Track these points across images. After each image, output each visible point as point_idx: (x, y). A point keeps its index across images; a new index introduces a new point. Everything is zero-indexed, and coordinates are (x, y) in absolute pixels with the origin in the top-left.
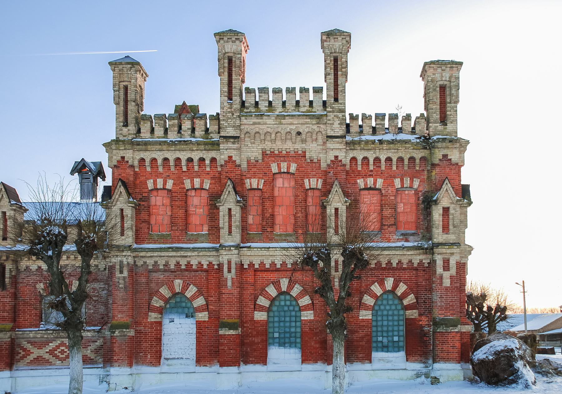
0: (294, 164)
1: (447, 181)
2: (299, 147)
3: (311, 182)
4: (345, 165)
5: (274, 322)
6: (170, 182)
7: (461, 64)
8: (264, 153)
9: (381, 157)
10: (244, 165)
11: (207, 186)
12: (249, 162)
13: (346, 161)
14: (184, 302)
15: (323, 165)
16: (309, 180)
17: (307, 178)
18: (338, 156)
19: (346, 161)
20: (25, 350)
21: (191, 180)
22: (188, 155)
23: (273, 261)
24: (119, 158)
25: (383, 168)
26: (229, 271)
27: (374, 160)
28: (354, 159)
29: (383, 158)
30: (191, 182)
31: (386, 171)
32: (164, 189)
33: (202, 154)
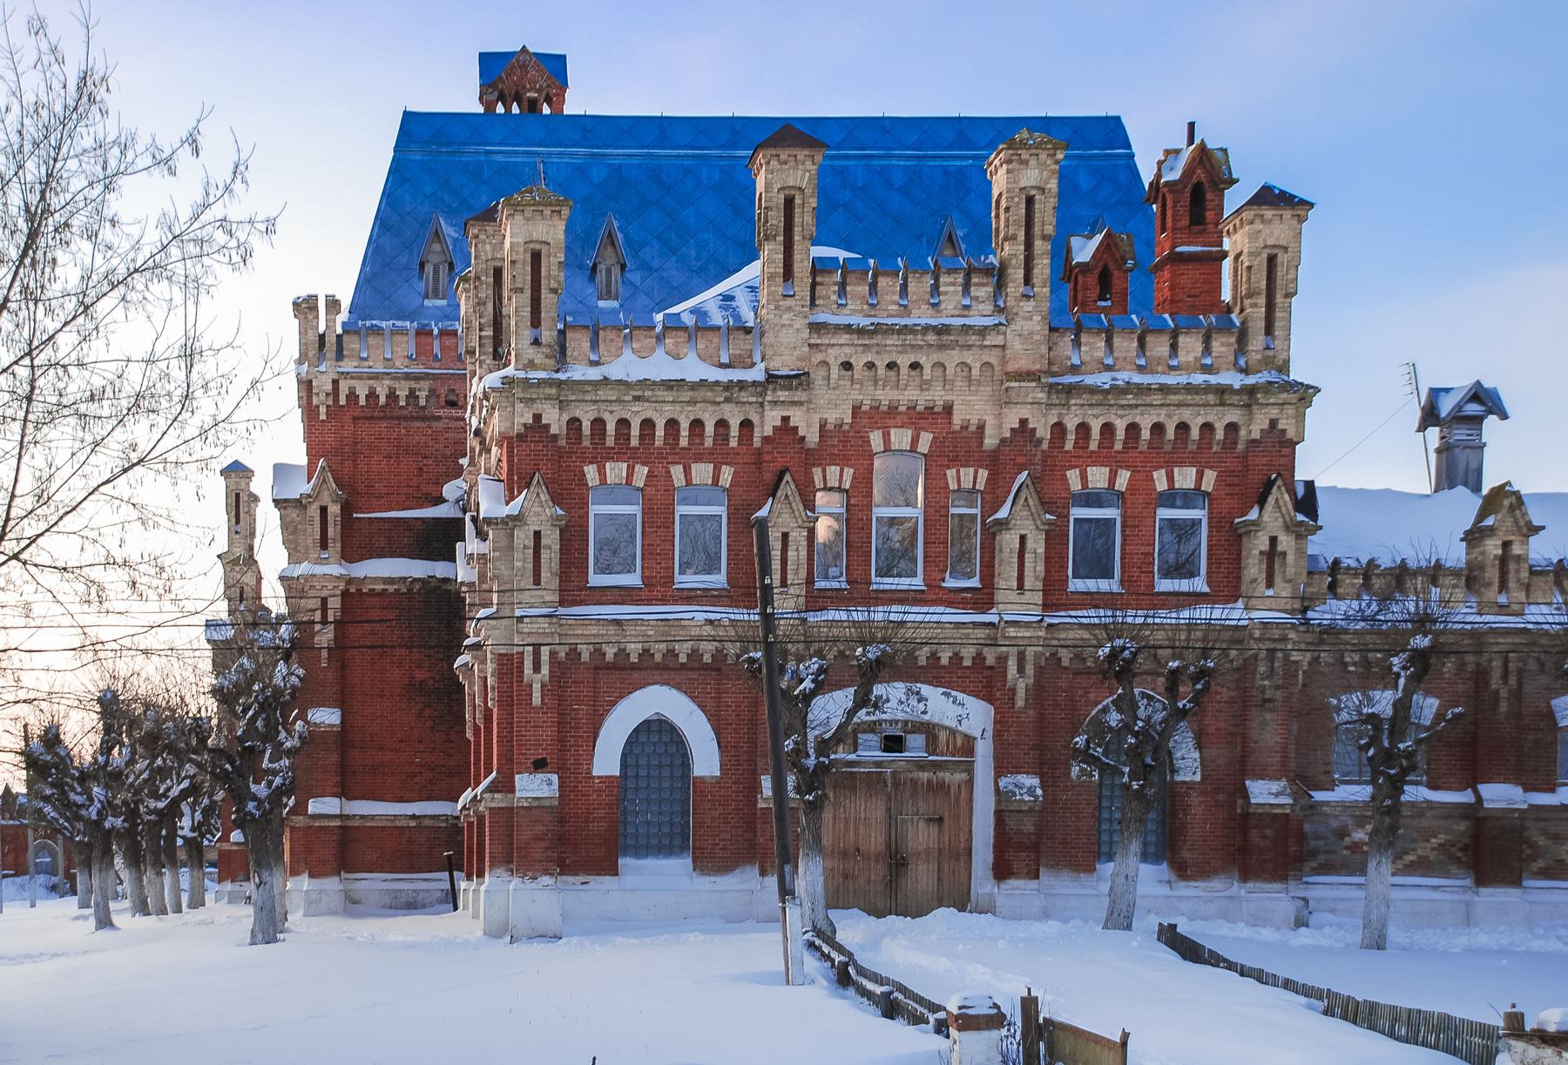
0: (876, 433)
1: (787, 477)
2: (938, 396)
3: (962, 474)
4: (1040, 441)
5: (672, 778)
6: (591, 470)
7: (1311, 205)
8: (856, 410)
9: (606, 416)
10: (813, 438)
11: (1209, 483)
12: (822, 426)
13: (1043, 432)
14: (649, 738)
15: (990, 441)
16: (824, 472)
17: (819, 465)
18: (789, 417)
19: (1043, 432)
20: (1533, 845)
21: (715, 468)
22: (669, 411)
23: (671, 647)
24: (1266, 425)
25: (733, 443)
26: (537, 668)
27: (1127, 429)
28: (574, 423)
29: (1071, 423)
30: (1087, 482)
31: (1150, 453)
32: (959, 490)
33: (1155, 416)
